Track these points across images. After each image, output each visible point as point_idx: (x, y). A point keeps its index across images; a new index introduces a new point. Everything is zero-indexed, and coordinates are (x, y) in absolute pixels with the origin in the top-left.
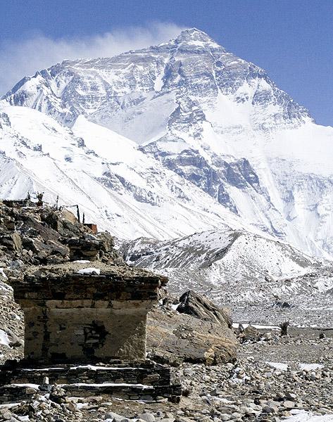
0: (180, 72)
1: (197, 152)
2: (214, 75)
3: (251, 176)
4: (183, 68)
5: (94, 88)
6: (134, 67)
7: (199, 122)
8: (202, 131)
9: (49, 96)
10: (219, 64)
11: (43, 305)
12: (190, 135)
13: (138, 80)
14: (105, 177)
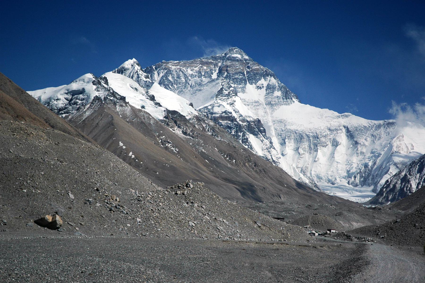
0: (227, 71)
1: (231, 113)
2: (245, 73)
4: (229, 69)
5: (179, 77)
6: (202, 67)
7: (233, 97)
8: (235, 102)
9: (138, 71)
10: (248, 67)
12: (228, 104)
13: (203, 74)
14: (164, 119)
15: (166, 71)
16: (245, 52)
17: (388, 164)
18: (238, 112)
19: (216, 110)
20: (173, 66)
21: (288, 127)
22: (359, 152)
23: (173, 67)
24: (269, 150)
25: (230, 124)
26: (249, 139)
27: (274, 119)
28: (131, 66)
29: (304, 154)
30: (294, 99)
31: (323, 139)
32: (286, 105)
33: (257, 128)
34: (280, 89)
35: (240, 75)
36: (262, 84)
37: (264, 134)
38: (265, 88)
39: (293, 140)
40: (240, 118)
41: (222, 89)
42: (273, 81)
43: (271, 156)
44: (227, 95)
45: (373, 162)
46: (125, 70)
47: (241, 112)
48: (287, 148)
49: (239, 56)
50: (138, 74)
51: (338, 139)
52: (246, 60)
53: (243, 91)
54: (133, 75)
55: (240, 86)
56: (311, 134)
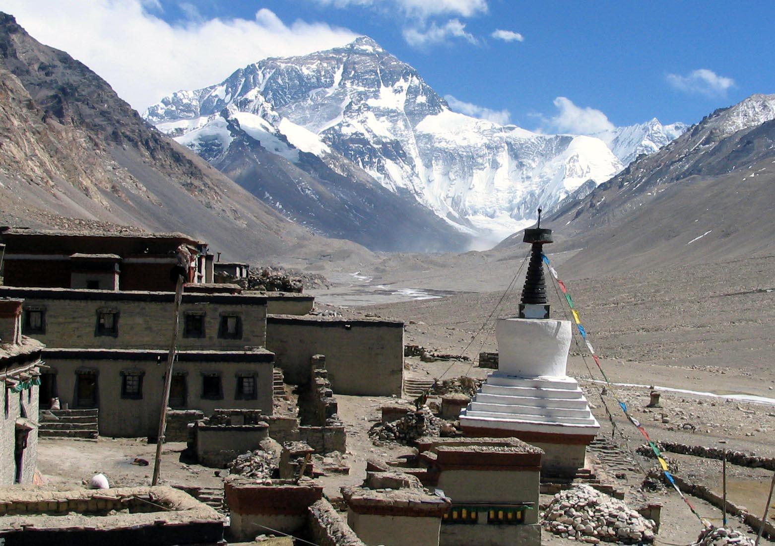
0: (354, 69)
1: (362, 134)
2: (379, 72)
3: (401, 152)
4: (356, 66)
7: (365, 113)
10: (383, 63)
11: (7, 34)
12: (358, 122)
15: (274, 70)
16: (378, 42)
17: (558, 193)
18: (372, 131)
19: (345, 130)
20: (282, 63)
21: (437, 145)
22: (525, 176)
23: (282, 64)
24: (411, 178)
25: (362, 148)
26: (386, 166)
27: (418, 133)
28: (254, 98)
29: (455, 179)
30: (443, 107)
31: (480, 160)
32: (432, 114)
33: (394, 150)
34: (425, 92)
35: (372, 75)
36: (401, 87)
37: (404, 158)
38: (405, 92)
39: (441, 161)
40: (375, 139)
41: (350, 104)
42: (416, 81)
43: (413, 185)
44: (357, 110)
45: (540, 189)
46: (248, 102)
47: (375, 132)
48: (434, 171)
49: (370, 49)
50: (263, 107)
51: (499, 159)
52: (378, 53)
53: (376, 96)
54: (258, 108)
55: (372, 90)
56: (465, 154)
